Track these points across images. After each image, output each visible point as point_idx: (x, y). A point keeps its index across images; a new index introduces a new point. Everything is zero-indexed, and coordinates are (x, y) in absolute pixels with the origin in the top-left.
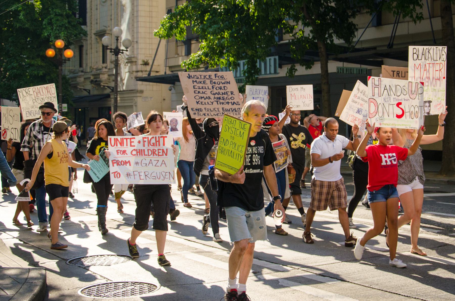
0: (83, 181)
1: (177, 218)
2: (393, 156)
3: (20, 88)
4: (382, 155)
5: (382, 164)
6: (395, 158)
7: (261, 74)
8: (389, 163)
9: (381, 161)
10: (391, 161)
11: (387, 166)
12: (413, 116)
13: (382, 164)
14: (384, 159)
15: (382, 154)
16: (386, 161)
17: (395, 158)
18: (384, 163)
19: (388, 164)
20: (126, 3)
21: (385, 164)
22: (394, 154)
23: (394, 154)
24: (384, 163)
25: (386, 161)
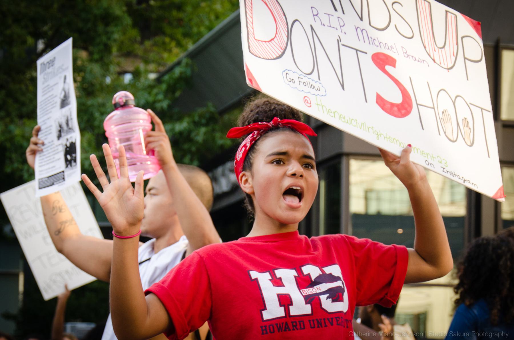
0: (259, 279)
1: (336, 275)
2: (332, 278)
3: (303, 266)
4: (263, 279)
5: (267, 315)
6: (339, 284)
7: (124, 146)
8: (300, 308)
9: (261, 304)
10: (313, 301)
11: (288, 323)
12: (451, 128)
13: (267, 315)
14: (270, 293)
15: (262, 269)
16: (285, 301)
17: (339, 284)
18: (273, 311)
19: (294, 311)
20: (157, 171)
21: (280, 312)
22: (335, 270)
23: (335, 270)
24: (273, 311)
25: (285, 301)
